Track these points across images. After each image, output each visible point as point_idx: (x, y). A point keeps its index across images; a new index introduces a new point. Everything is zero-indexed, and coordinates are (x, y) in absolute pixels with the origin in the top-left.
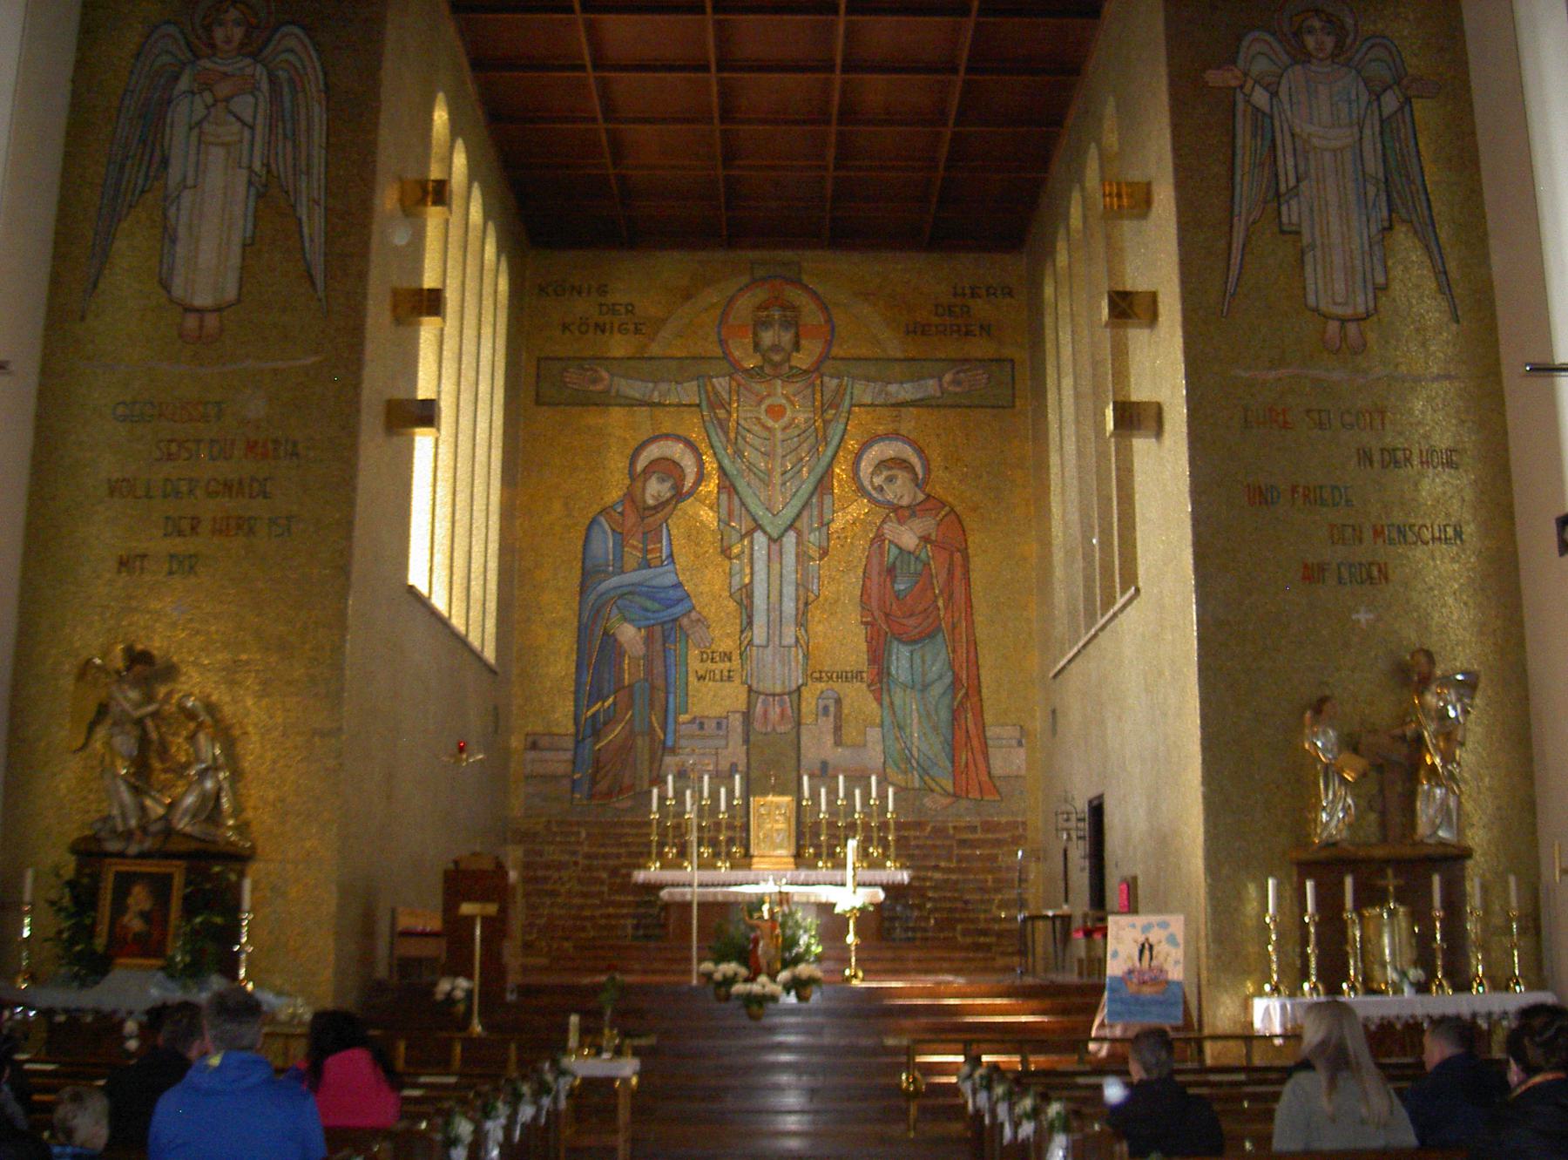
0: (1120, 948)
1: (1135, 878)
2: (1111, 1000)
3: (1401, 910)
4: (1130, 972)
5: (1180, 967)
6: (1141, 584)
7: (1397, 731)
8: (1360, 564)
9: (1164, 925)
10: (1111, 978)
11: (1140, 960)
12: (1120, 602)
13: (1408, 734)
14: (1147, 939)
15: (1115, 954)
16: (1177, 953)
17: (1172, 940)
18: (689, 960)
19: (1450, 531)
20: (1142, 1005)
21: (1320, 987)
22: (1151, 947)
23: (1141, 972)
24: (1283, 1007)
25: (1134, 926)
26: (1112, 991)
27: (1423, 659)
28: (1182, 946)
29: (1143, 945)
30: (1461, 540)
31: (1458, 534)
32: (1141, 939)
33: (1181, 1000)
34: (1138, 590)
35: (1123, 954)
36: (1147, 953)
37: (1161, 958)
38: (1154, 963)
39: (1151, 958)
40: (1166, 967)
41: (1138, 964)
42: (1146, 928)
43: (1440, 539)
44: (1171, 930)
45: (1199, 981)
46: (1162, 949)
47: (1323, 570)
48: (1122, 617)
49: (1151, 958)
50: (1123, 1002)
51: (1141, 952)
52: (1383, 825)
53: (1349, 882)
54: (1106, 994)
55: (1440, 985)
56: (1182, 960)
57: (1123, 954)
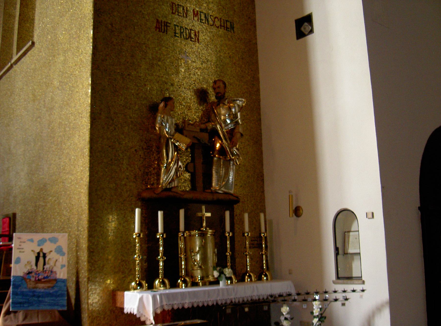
0: (22, 256)
1: (14, 215)
2: (14, 294)
3: (210, 231)
4: (29, 273)
5: (65, 269)
6: (35, 39)
7: (203, 126)
8: (186, 28)
9: (54, 240)
10: (13, 276)
11: (36, 265)
12: (15, 58)
13: (209, 128)
14: (41, 250)
15: (18, 261)
16: (63, 260)
17: (59, 251)
18: (218, 290)
19: (229, 24)
20: (39, 297)
21: (166, 281)
22: (44, 256)
23: (37, 273)
24: (154, 298)
25: (32, 240)
26: (15, 286)
27: (222, 85)
28: (66, 255)
29: (39, 253)
30: (233, 30)
31: (232, 28)
32: (38, 250)
33: (66, 293)
34: (33, 43)
35: (24, 260)
36: (41, 259)
37: (52, 263)
38: (47, 266)
39: (44, 264)
40: (55, 269)
41: (34, 267)
42: (42, 242)
43: (224, 26)
44: (58, 244)
45: (78, 278)
46: (52, 257)
47: (167, 26)
48: (15, 67)
49: (44, 264)
50: (23, 294)
51: (37, 258)
52: (193, 180)
53: (182, 212)
54: (11, 289)
55: (250, 276)
56: (66, 264)
57: (24, 260)
